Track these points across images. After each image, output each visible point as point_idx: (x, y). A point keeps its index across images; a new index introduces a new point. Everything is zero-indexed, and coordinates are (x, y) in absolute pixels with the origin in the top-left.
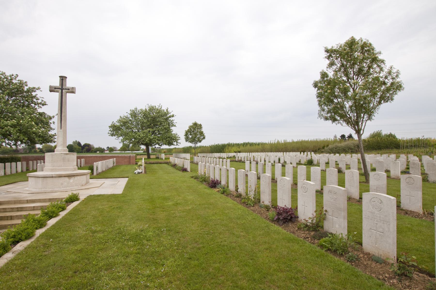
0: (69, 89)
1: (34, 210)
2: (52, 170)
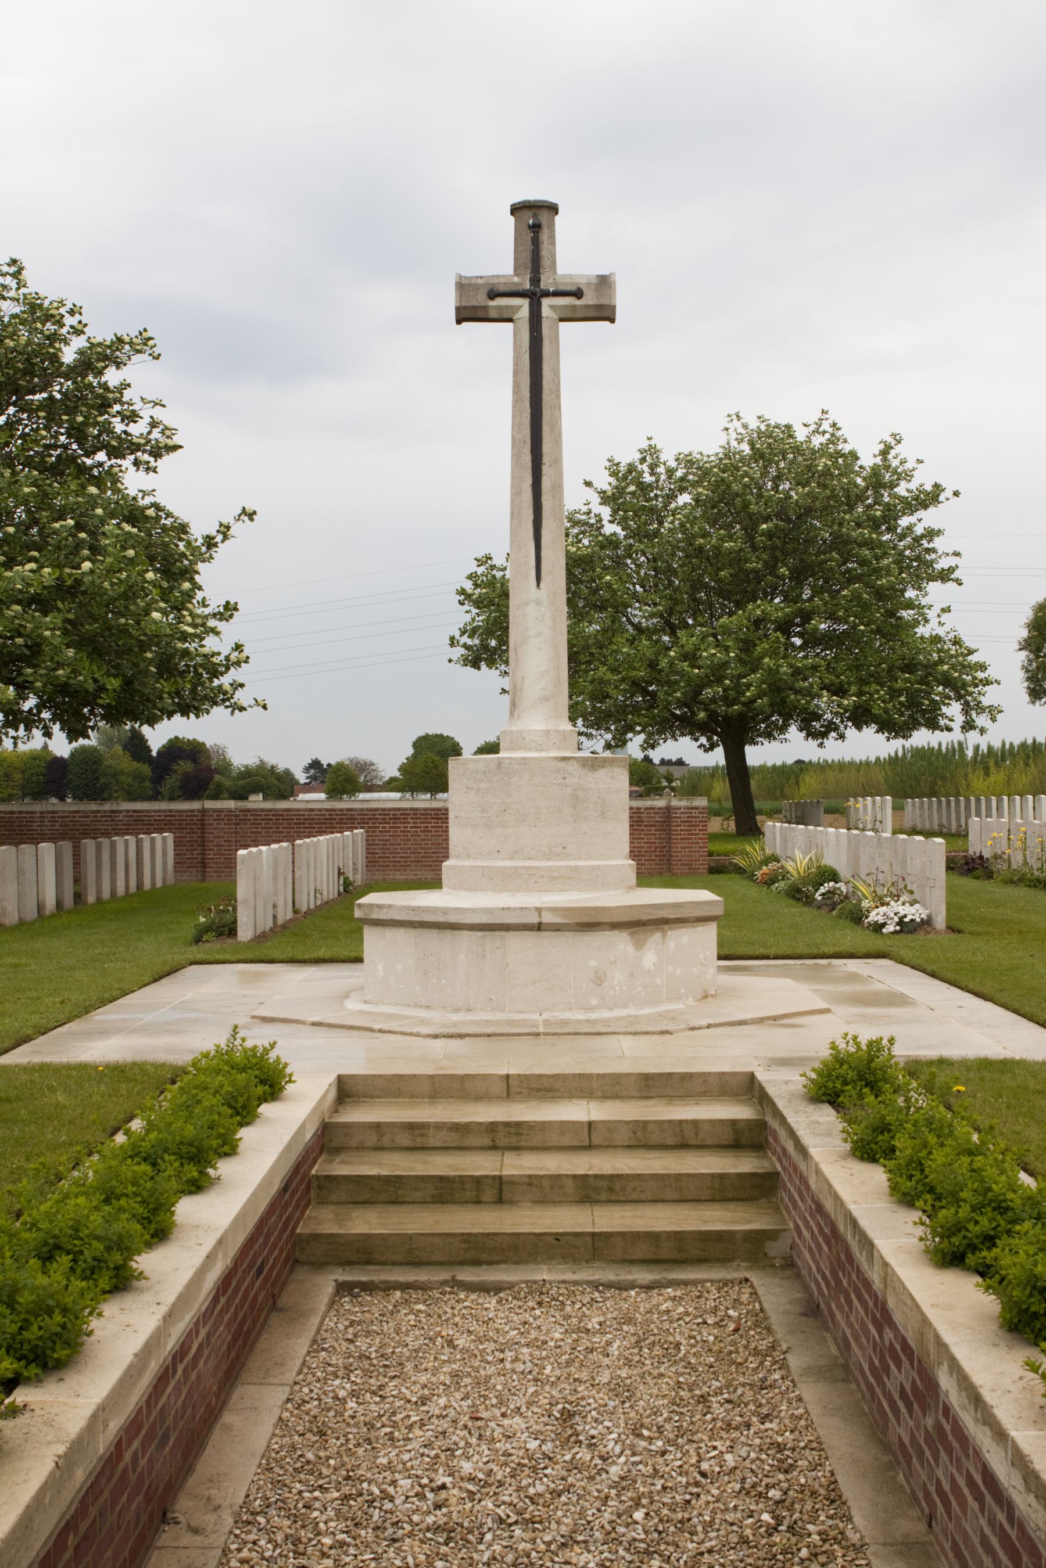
0: (578, 294)
1: (590, 1147)
2: (504, 880)
